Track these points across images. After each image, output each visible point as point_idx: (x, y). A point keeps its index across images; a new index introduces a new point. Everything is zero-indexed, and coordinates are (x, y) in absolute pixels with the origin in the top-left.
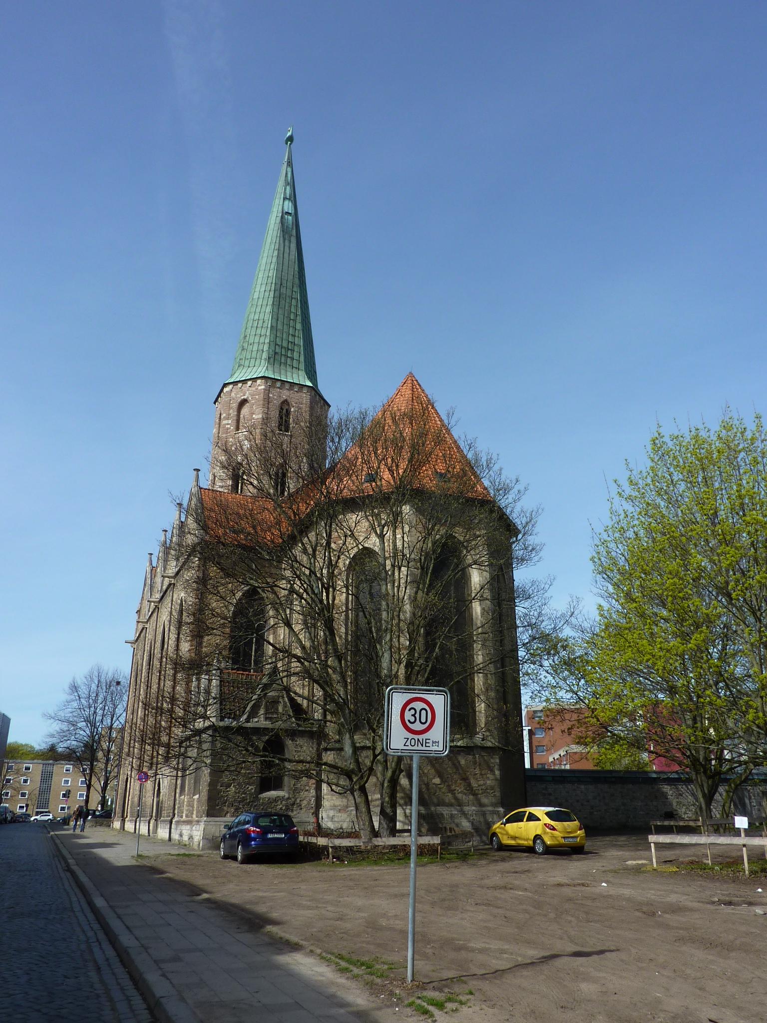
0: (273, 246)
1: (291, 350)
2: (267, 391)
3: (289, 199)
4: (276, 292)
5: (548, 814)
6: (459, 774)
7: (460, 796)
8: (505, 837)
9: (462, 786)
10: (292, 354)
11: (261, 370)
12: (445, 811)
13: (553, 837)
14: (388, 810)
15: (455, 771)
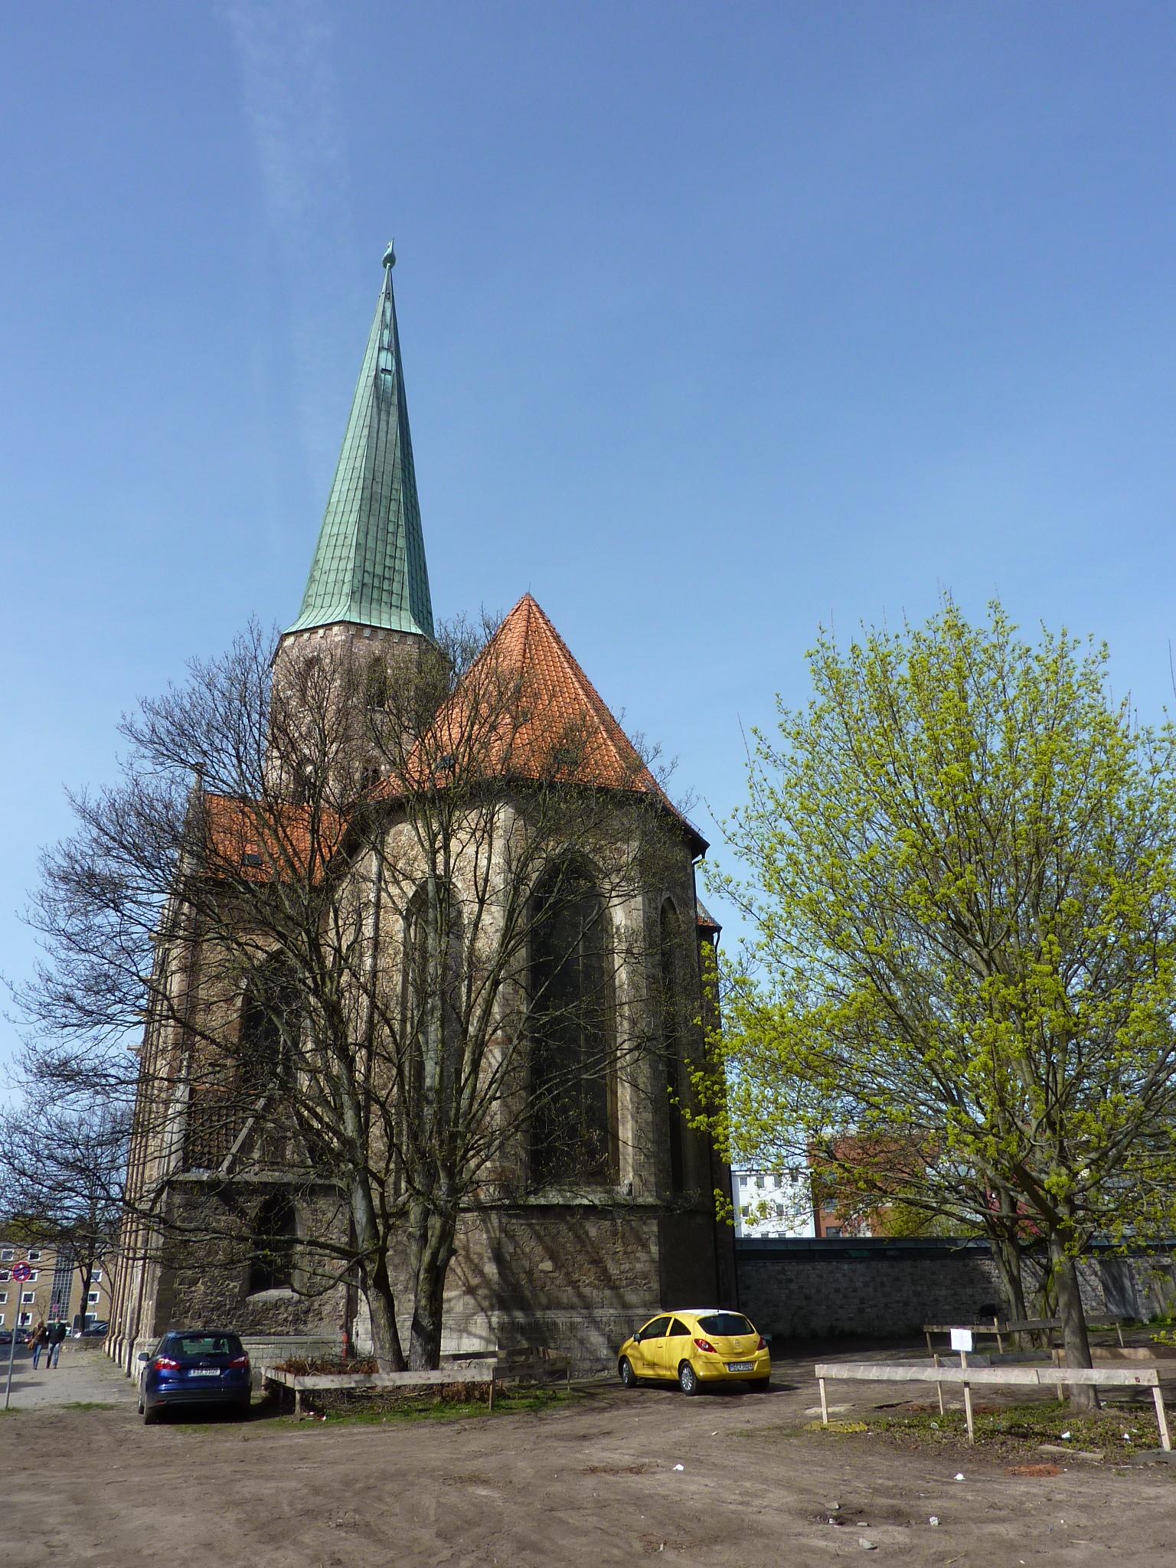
0: (362, 422)
1: (389, 579)
2: (350, 643)
3: (388, 350)
4: (366, 491)
5: (705, 1323)
6: (587, 1252)
7: (587, 1291)
8: (640, 1364)
9: (592, 1274)
10: (391, 585)
11: (341, 610)
12: (561, 1318)
13: (709, 1363)
14: (426, 1322)
15: (578, 1247)
